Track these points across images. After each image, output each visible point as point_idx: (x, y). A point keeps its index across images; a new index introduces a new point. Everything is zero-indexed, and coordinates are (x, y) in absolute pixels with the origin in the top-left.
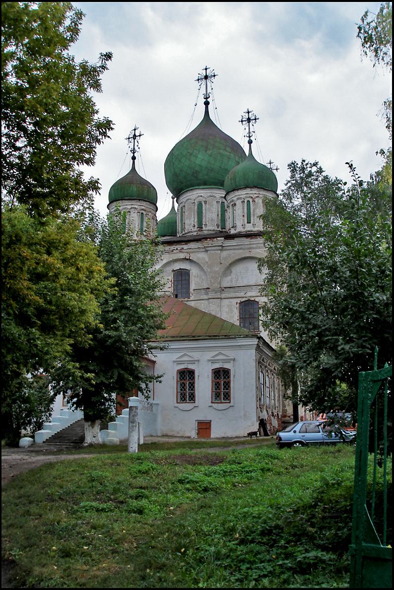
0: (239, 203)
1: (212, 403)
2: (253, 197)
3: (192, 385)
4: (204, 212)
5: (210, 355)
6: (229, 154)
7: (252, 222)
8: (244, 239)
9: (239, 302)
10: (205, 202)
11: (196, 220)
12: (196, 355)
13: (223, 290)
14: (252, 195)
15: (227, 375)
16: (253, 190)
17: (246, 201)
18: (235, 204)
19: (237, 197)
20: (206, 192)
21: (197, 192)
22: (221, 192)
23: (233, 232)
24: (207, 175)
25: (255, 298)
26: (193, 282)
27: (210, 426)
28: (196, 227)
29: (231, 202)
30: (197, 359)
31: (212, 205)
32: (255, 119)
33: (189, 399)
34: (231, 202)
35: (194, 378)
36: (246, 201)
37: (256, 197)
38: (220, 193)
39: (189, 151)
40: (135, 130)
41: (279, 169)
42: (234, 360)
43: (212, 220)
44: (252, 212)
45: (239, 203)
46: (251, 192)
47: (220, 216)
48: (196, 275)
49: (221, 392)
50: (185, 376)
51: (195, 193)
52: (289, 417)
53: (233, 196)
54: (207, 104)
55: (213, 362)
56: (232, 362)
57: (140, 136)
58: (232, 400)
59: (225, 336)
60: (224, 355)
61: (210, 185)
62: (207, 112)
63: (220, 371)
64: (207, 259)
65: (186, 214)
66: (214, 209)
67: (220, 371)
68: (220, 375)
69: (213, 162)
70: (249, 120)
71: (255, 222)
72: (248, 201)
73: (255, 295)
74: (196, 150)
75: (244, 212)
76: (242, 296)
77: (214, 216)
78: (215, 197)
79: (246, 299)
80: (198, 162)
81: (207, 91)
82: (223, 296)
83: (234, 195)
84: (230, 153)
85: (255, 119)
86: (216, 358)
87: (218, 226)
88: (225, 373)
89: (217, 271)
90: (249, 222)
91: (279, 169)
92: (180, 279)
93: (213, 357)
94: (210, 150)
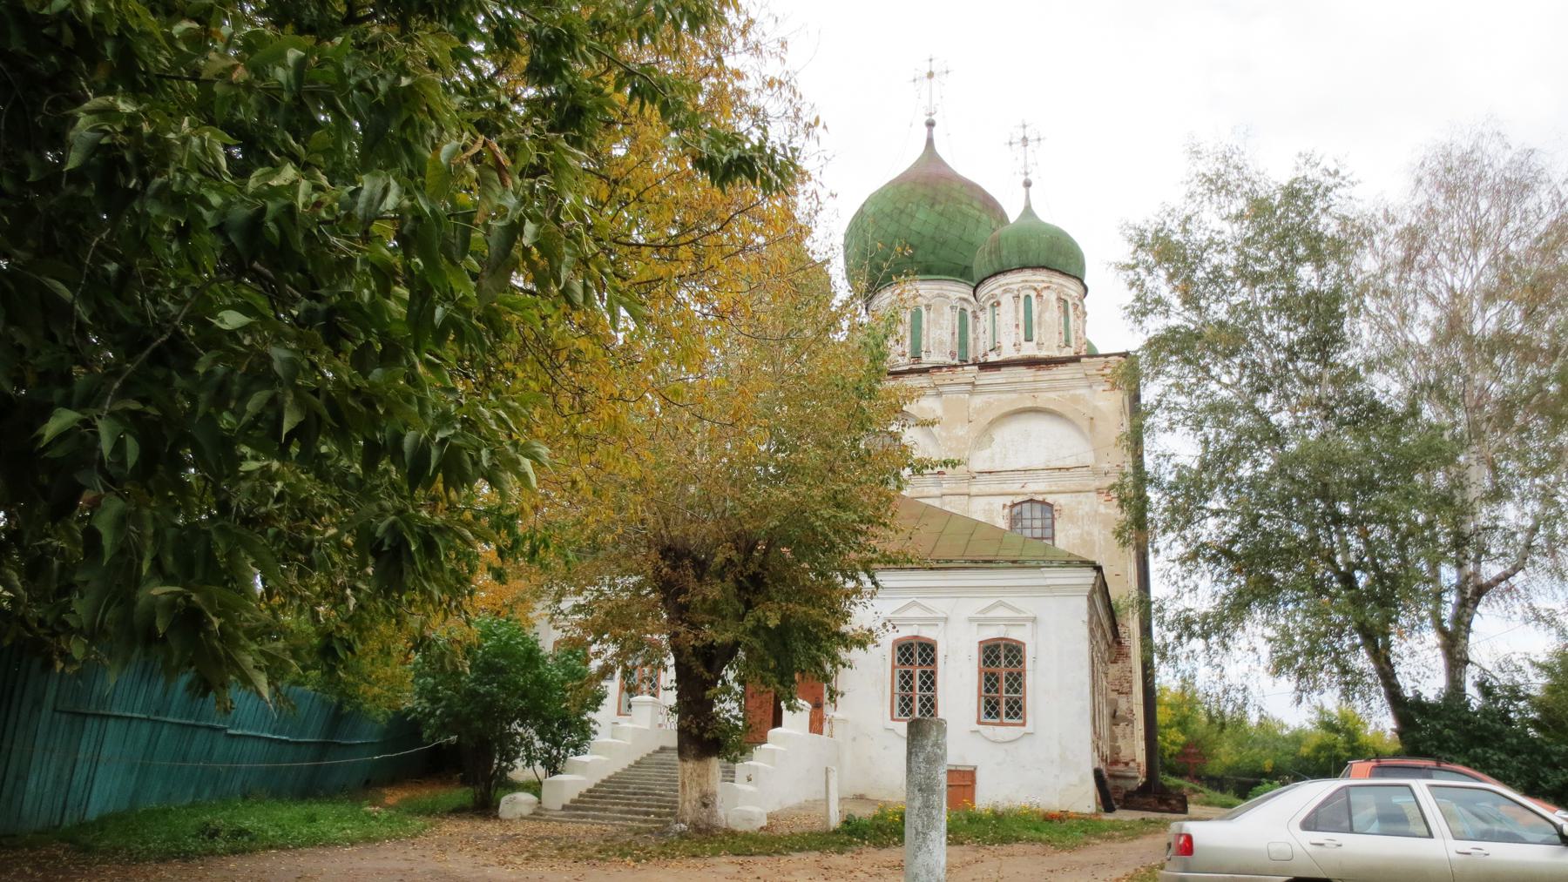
0: (1007, 300)
1: (979, 722)
3: (929, 677)
4: (924, 326)
5: (974, 606)
7: (1035, 338)
8: (1022, 370)
9: (1009, 504)
10: (928, 307)
12: (940, 606)
14: (1035, 285)
15: (1015, 657)
17: (1022, 296)
18: (999, 304)
23: (992, 358)
24: (933, 253)
27: (973, 781)
28: (908, 355)
29: (989, 298)
34: (989, 298)
35: (933, 661)
36: (1022, 296)
38: (957, 291)
42: (1034, 620)
43: (941, 343)
44: (1035, 318)
45: (1007, 300)
46: (1034, 278)
47: (957, 336)
49: (1001, 697)
53: (991, 287)
55: (982, 623)
56: (1029, 625)
58: (1029, 718)
59: (1014, 562)
60: (1012, 608)
62: (930, 142)
63: (998, 646)
67: (998, 646)
68: (998, 657)
72: (1028, 297)
73: (1048, 489)
75: (1017, 319)
76: (1018, 491)
77: (946, 336)
79: (1026, 498)
82: (974, 490)
85: (1039, 140)
86: (903, 615)
87: (953, 354)
88: (1010, 651)
90: (1029, 339)
93: (981, 612)
94: (940, 203)
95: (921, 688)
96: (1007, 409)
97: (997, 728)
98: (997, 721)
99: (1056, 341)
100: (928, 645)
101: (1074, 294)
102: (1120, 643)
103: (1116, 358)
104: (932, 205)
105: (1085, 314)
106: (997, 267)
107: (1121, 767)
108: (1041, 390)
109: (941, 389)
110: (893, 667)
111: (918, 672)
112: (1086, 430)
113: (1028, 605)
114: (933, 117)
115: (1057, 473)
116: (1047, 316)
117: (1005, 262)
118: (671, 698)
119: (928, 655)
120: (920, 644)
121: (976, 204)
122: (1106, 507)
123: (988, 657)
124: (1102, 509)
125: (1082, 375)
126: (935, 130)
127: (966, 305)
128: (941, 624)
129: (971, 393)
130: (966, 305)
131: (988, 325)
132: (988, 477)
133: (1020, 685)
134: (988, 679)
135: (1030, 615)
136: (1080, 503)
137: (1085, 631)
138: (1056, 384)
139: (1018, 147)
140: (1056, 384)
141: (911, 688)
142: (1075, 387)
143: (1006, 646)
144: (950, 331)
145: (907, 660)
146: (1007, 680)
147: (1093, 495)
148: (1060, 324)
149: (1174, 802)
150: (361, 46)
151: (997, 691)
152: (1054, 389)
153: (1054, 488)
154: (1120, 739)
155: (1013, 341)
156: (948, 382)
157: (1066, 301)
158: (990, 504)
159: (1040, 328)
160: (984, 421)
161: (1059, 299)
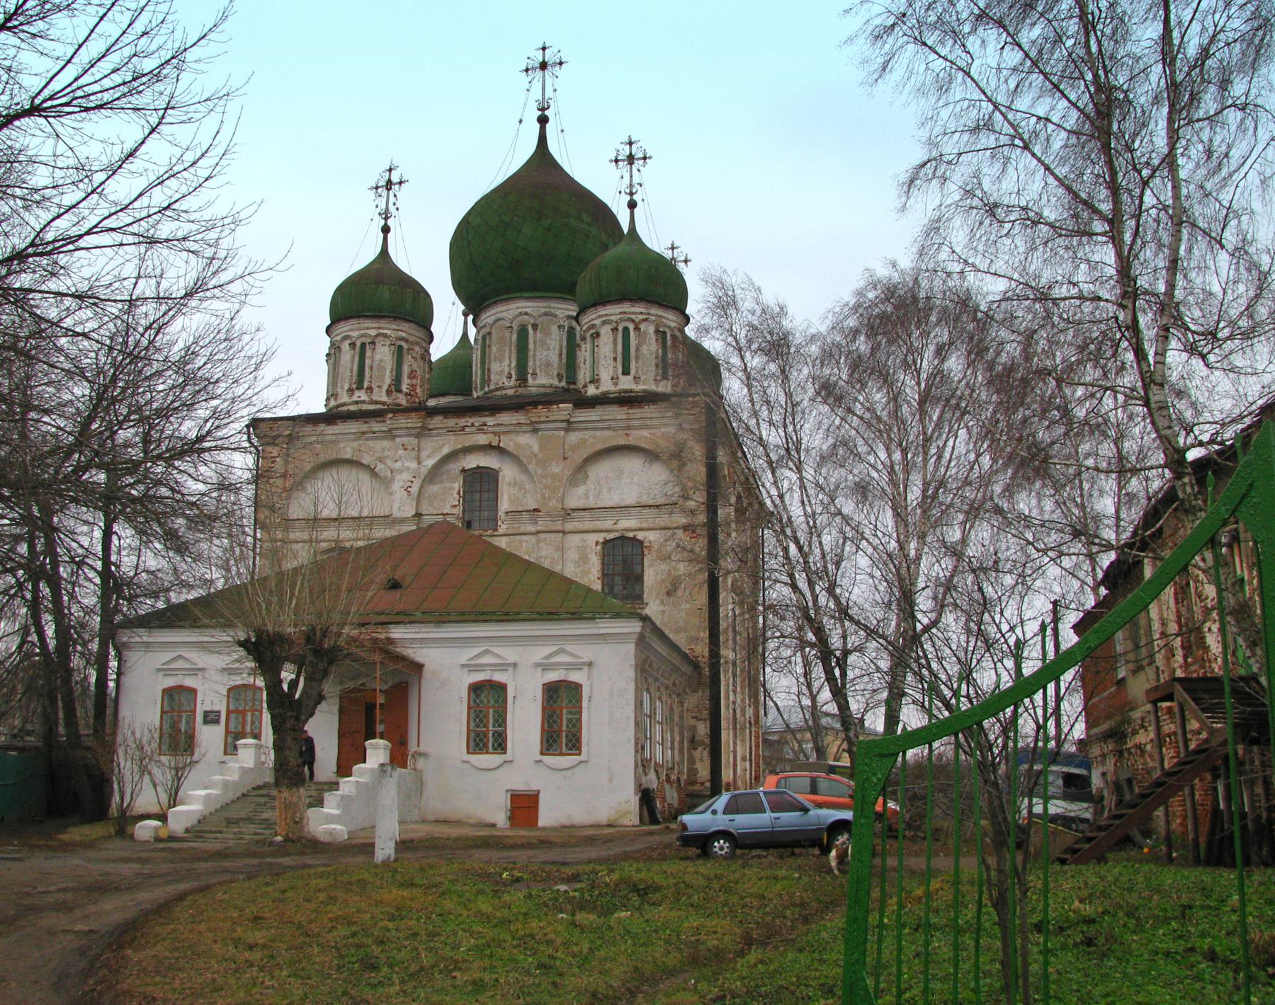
0: (605, 331)
4: (531, 346)
7: (633, 371)
11: (514, 364)
14: (633, 317)
17: (620, 328)
18: (598, 335)
26: (506, 497)
34: (589, 328)
36: (620, 328)
38: (564, 310)
40: (390, 170)
41: (371, 189)
42: (590, 664)
43: (548, 365)
45: (605, 331)
46: (633, 310)
47: (564, 356)
52: (702, 784)
54: (543, 120)
56: (586, 669)
57: (400, 183)
59: (573, 614)
64: (536, 449)
65: (494, 349)
70: (631, 159)
73: (639, 526)
75: (615, 351)
78: (555, 316)
82: (569, 526)
85: (645, 158)
87: (560, 377)
90: (626, 372)
91: (371, 189)
96: (600, 446)
99: (653, 374)
101: (673, 325)
108: (635, 428)
113: (585, 652)
114: (546, 113)
116: (644, 349)
129: (567, 430)
131: (588, 355)
132: (583, 513)
135: (586, 660)
137: (631, 673)
138: (648, 422)
140: (648, 422)
144: (557, 352)
152: (647, 427)
153: (645, 525)
156: (543, 419)
158: (583, 540)
159: (637, 362)
160: (578, 458)
161: (657, 331)
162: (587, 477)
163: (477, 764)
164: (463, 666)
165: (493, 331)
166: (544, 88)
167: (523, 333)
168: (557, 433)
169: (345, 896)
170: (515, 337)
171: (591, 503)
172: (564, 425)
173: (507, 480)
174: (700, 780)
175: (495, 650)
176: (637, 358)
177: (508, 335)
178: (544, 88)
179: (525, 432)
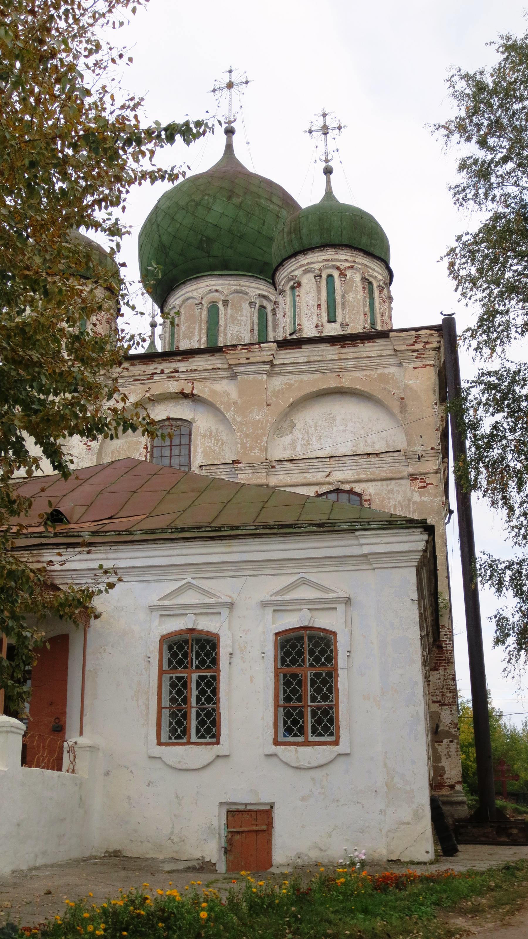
0: (308, 281)
1: (276, 743)
2: (342, 267)
4: (222, 322)
6: (278, 209)
7: (339, 319)
8: (325, 348)
10: (226, 303)
13: (273, 467)
14: (338, 264)
15: (323, 652)
16: (341, 252)
17: (324, 276)
18: (299, 284)
19: (304, 268)
20: (227, 282)
21: (207, 283)
22: (259, 286)
25: (352, 485)
26: (200, 450)
27: (270, 824)
29: (289, 280)
30: (229, 600)
31: (241, 310)
32: (340, 128)
33: (198, 731)
35: (215, 662)
36: (324, 276)
37: (348, 267)
39: (193, 197)
42: (348, 601)
44: (338, 298)
45: (308, 281)
46: (337, 257)
47: (256, 332)
48: (208, 433)
49: (306, 706)
50: (186, 655)
51: (204, 284)
52: (452, 787)
56: (341, 608)
59: (320, 525)
61: (237, 270)
62: (229, 147)
63: (300, 639)
64: (234, 396)
65: (183, 328)
66: (245, 319)
67: (300, 639)
68: (300, 653)
69: (244, 221)
70: (325, 130)
71: (347, 320)
73: (356, 477)
74: (208, 195)
75: (319, 299)
76: (323, 480)
78: (246, 294)
79: (331, 488)
80: (211, 218)
81: (230, 110)
83: (298, 265)
84: (281, 207)
85: (340, 128)
86: (289, 596)
88: (317, 645)
89: (259, 420)
90: (332, 320)
92: (168, 443)
94: (238, 196)
95: (198, 700)
97: (301, 749)
98: (301, 739)
100: (208, 641)
101: (380, 277)
102: (440, 647)
103: (428, 331)
104: (230, 198)
105: (391, 299)
106: (297, 247)
107: (445, 791)
108: (347, 369)
109: (236, 369)
110: (161, 672)
111: (194, 677)
112: (396, 410)
115: (365, 459)
116: (351, 296)
117: (305, 241)
118: (65, 744)
119: (207, 655)
120: (198, 641)
121: (275, 199)
122: (421, 495)
123: (287, 654)
124: (416, 497)
125: (391, 352)
126: (235, 138)
127: (265, 303)
128: (225, 612)
129: (269, 374)
130: (265, 303)
131: (288, 309)
132: (289, 465)
133: (330, 689)
134: (287, 684)
136: (391, 492)
138: (363, 362)
139: (318, 136)
140: (363, 362)
141: (185, 700)
142: (383, 366)
143: (311, 638)
144: (249, 328)
145: (180, 663)
146: (313, 683)
147: (406, 483)
148: (364, 305)
149: (515, 831)
150: (338, 801)
151: (299, 699)
152: (362, 368)
153: (363, 476)
154: (443, 759)
155: (315, 322)
157: (370, 283)
159: (343, 308)
160: (284, 403)
161: (364, 279)
162: (293, 425)
163: (171, 761)
164: (152, 608)
165: (182, 310)
166: (230, 104)
167: (213, 310)
168: (259, 377)
169: (397, 488)
170: (205, 313)
171: (299, 452)
172: (267, 367)
173: (202, 431)
174: (448, 782)
175: (205, 584)
176: (343, 304)
177: (197, 312)
178: (230, 104)
179: (222, 378)
